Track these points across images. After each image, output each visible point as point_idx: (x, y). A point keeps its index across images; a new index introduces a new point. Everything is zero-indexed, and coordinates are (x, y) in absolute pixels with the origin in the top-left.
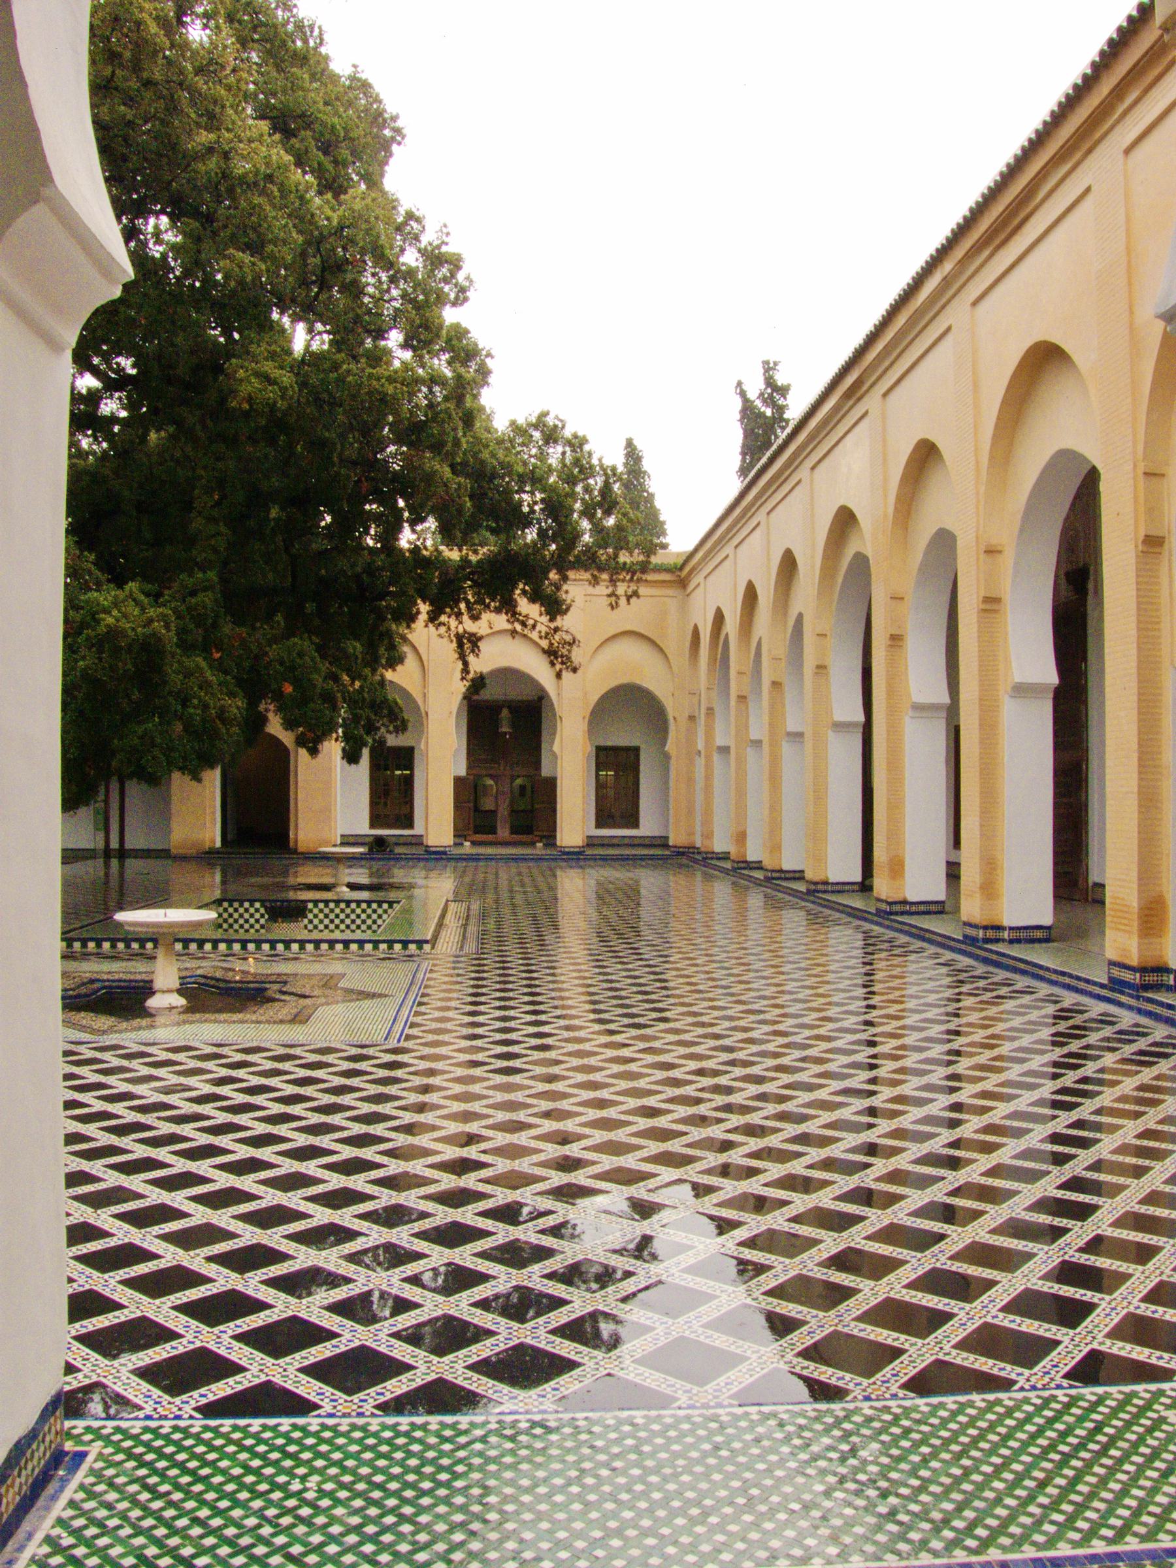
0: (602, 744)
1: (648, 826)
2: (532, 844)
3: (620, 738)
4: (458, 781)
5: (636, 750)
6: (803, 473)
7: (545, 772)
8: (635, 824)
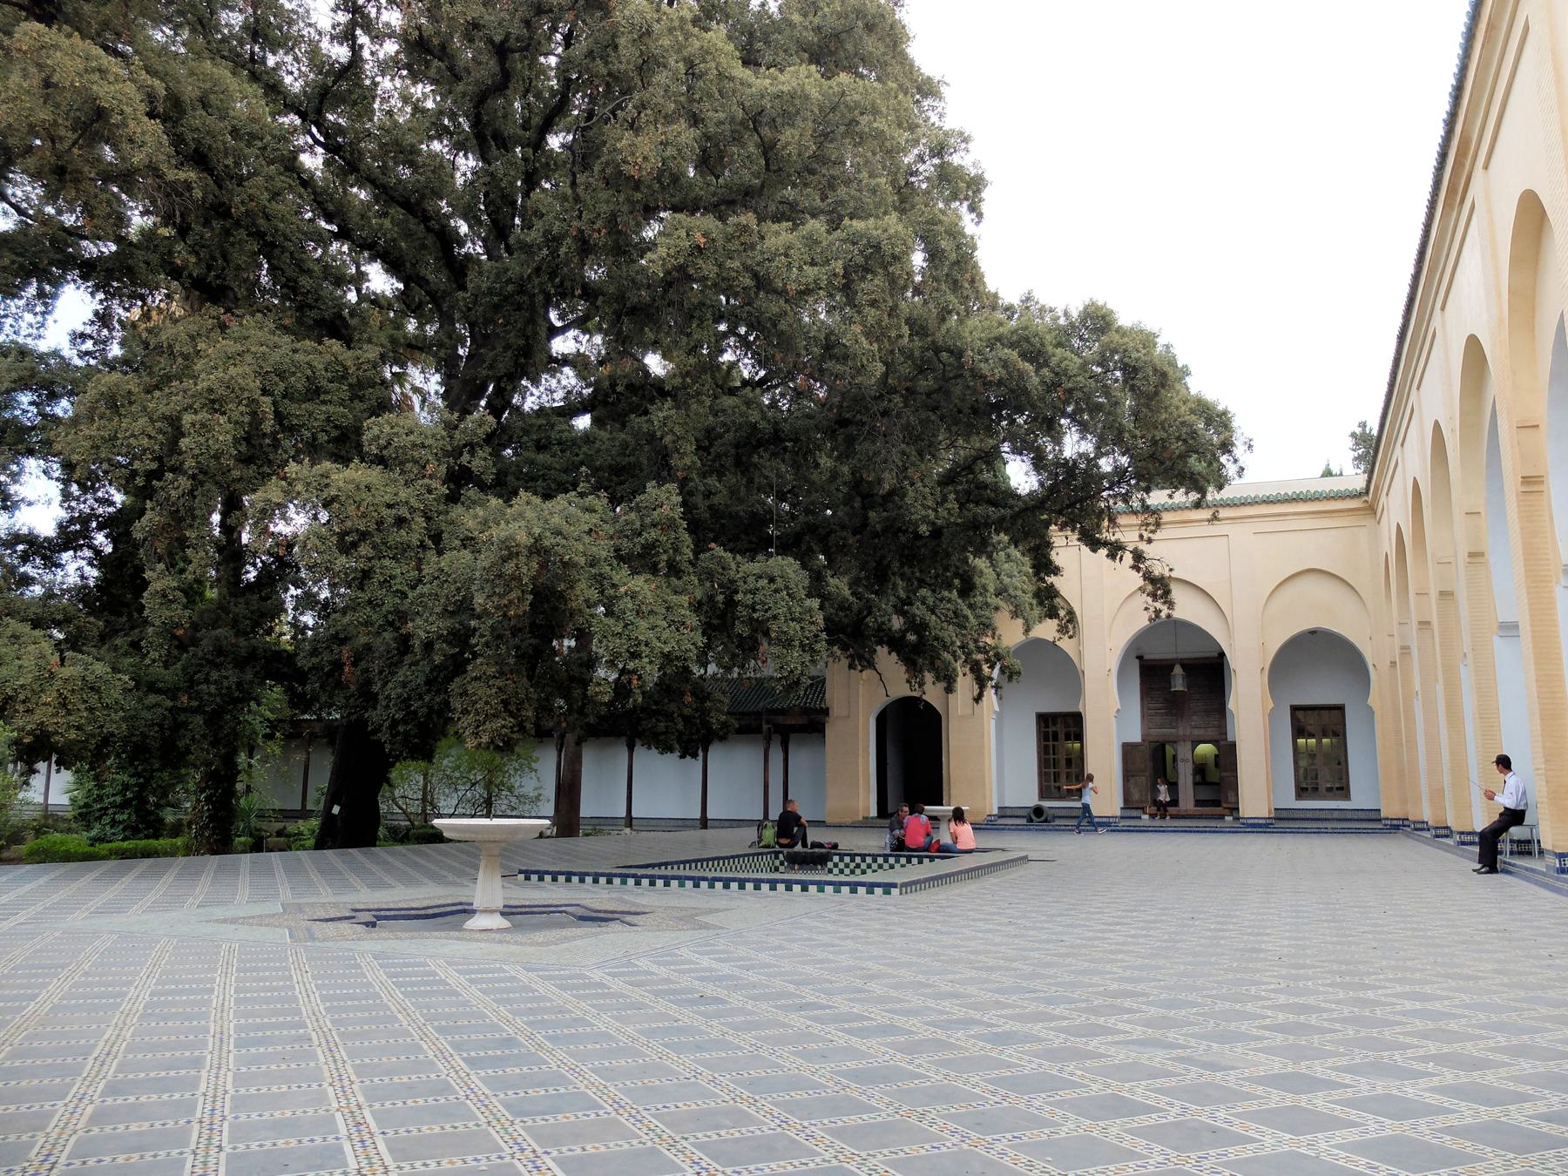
0: (1296, 703)
1: (1360, 798)
2: (1221, 817)
3: (1319, 693)
4: (1128, 750)
5: (1340, 709)
6: (1436, 322)
7: (1230, 739)
8: (1347, 797)
